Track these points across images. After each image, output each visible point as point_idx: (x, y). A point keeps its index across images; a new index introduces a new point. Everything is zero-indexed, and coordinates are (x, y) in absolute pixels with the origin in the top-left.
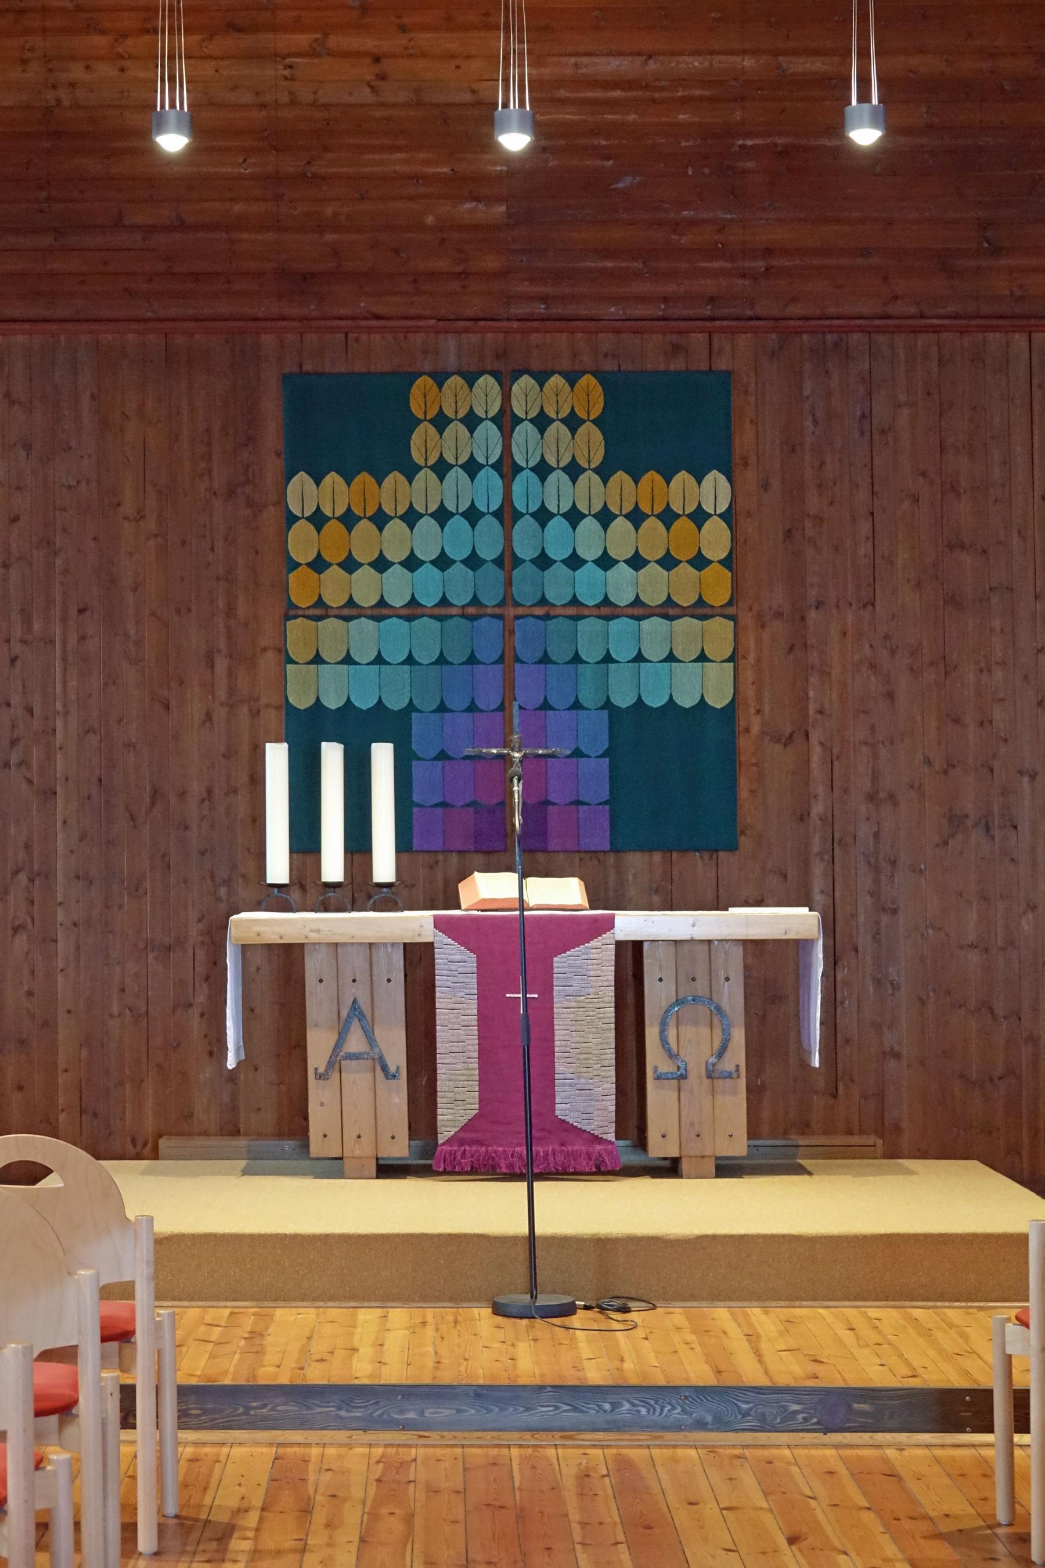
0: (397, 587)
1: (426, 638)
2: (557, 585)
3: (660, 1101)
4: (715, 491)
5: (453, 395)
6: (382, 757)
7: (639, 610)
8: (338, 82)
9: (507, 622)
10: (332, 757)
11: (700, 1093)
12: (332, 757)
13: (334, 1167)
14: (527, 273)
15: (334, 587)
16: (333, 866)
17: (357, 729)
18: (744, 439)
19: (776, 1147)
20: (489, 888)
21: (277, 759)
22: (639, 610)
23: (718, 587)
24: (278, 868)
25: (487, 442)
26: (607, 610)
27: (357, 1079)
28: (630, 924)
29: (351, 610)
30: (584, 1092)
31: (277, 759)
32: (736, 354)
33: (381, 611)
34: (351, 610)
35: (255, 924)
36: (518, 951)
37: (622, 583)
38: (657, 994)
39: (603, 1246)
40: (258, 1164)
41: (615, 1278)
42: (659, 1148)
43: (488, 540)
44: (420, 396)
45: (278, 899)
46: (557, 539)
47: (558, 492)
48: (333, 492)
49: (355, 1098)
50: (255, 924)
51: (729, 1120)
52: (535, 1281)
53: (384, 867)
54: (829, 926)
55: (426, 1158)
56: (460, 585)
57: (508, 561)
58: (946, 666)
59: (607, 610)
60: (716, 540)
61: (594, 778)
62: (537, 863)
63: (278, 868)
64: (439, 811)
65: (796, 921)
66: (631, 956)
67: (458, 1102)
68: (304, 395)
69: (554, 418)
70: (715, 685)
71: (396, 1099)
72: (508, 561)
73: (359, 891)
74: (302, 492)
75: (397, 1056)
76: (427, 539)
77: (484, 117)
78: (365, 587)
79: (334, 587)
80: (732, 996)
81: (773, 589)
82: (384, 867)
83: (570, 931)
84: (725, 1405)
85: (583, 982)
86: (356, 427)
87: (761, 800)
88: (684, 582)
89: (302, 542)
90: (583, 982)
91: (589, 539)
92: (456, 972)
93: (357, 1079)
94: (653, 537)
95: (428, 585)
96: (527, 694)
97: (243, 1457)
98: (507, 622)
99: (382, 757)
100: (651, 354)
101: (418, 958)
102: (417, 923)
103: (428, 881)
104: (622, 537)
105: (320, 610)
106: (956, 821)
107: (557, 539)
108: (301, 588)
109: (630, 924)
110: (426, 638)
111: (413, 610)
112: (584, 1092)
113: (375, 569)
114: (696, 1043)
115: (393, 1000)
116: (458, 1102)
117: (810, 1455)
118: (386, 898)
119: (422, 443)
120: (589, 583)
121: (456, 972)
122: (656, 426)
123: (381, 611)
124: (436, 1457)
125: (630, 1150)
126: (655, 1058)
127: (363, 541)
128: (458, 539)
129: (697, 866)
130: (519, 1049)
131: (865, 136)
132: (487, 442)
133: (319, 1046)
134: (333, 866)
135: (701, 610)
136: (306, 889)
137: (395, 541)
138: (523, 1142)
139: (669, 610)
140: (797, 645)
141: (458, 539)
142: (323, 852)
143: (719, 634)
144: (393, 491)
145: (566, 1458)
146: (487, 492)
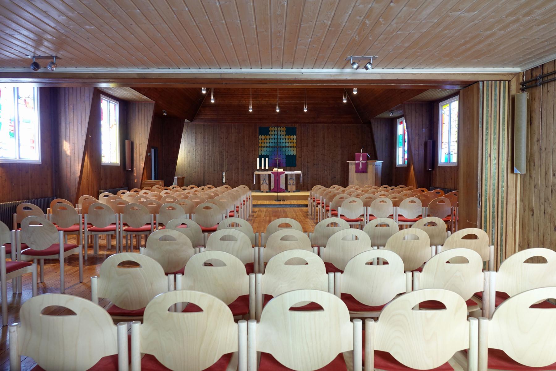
0: (268, 145)
1: (271, 149)
2: (281, 145)
3: (289, 186)
4: (295, 137)
5: (273, 129)
6: (267, 159)
7: (288, 147)
8: (264, 102)
9: (277, 148)
10: (263, 159)
11: (292, 185)
12: (263, 159)
13: (263, 192)
14: (278, 120)
15: (263, 145)
16: (263, 168)
17: (265, 157)
18: (297, 132)
19: (298, 190)
20: (275, 170)
21: (258, 159)
22: (288, 147)
23: (295, 145)
24: (258, 168)
25: (276, 133)
26: (286, 147)
27: (264, 185)
28: (286, 172)
29: (264, 147)
30: (283, 186)
31: (258, 159)
32: (297, 125)
33: (267, 147)
34: (264, 147)
35: (256, 172)
36: (278, 174)
37: (287, 145)
38: (289, 178)
39: (283, 196)
40: (256, 192)
41: (284, 199)
42: (289, 190)
43: (276, 141)
44: (270, 129)
45: (258, 170)
46: (282, 141)
47: (282, 137)
48: (263, 137)
49: (264, 187)
50: (256, 172)
51: (294, 188)
52: (278, 199)
53: (267, 168)
54: (303, 173)
55: (270, 191)
56: (273, 145)
57: (277, 143)
58: (313, 151)
59: (286, 147)
60: (295, 141)
61: (284, 161)
62: (279, 168)
63: (258, 168)
64: (448, 186)
65: (300, 172)
66: (286, 175)
67: (273, 186)
68: (260, 128)
69: (282, 130)
70: (294, 153)
71: (268, 186)
72: (277, 143)
73: (265, 170)
74: (260, 137)
75: (268, 183)
76: (271, 141)
77: (274, 107)
78: (265, 145)
79: (263, 145)
80: (294, 178)
81: (300, 145)
82: (267, 168)
83: (282, 173)
84: (291, 206)
85: (283, 177)
86: (265, 131)
87: (298, 163)
88: (292, 145)
89: (260, 141)
90: (283, 177)
91: (284, 141)
92: (273, 177)
93: (264, 185)
94: (290, 141)
95: (271, 145)
96: (279, 153)
97: (257, 209)
98: (277, 148)
99: (267, 159)
100: (290, 125)
101: (270, 175)
102: (270, 172)
103: (270, 169)
104: (287, 141)
105: (262, 147)
106: (314, 164)
107: (282, 141)
108: (260, 145)
109: (286, 172)
110: (271, 149)
111: (269, 147)
112: (283, 186)
113: (266, 143)
114: (291, 182)
115: (267, 179)
116: (273, 186)
117: (296, 209)
118: (267, 170)
119: (270, 133)
120: (284, 145)
121: (273, 177)
122: (290, 131)
123: (267, 147)
124: (270, 209)
125: (286, 190)
126: (288, 183)
127: (265, 141)
128: (273, 141)
129: (293, 168)
130: (277, 182)
131: (305, 111)
132: (276, 133)
133: (261, 182)
134: (263, 168)
135: (293, 147)
136: (260, 170)
137: (268, 141)
138: (278, 189)
139: (291, 147)
140: (301, 150)
141: (273, 141)
142: (262, 164)
143: (295, 149)
144: (268, 137)
145: (279, 209)
146: (276, 137)
